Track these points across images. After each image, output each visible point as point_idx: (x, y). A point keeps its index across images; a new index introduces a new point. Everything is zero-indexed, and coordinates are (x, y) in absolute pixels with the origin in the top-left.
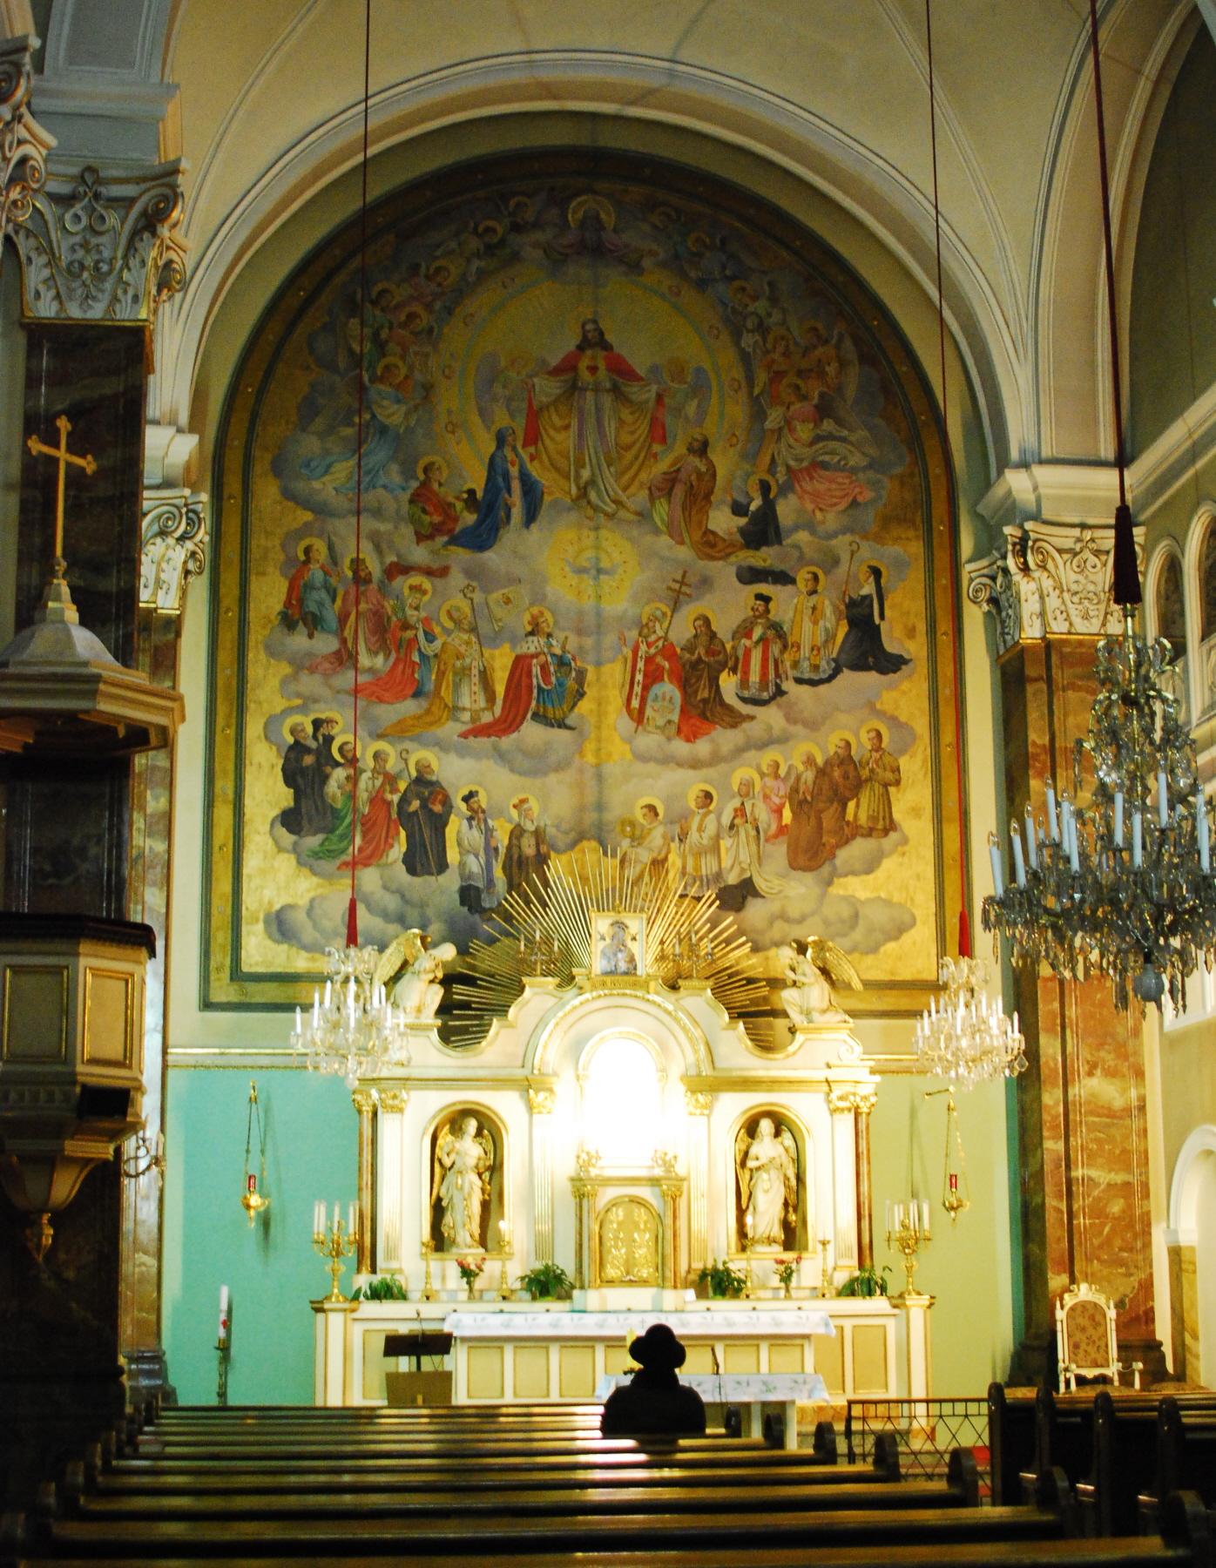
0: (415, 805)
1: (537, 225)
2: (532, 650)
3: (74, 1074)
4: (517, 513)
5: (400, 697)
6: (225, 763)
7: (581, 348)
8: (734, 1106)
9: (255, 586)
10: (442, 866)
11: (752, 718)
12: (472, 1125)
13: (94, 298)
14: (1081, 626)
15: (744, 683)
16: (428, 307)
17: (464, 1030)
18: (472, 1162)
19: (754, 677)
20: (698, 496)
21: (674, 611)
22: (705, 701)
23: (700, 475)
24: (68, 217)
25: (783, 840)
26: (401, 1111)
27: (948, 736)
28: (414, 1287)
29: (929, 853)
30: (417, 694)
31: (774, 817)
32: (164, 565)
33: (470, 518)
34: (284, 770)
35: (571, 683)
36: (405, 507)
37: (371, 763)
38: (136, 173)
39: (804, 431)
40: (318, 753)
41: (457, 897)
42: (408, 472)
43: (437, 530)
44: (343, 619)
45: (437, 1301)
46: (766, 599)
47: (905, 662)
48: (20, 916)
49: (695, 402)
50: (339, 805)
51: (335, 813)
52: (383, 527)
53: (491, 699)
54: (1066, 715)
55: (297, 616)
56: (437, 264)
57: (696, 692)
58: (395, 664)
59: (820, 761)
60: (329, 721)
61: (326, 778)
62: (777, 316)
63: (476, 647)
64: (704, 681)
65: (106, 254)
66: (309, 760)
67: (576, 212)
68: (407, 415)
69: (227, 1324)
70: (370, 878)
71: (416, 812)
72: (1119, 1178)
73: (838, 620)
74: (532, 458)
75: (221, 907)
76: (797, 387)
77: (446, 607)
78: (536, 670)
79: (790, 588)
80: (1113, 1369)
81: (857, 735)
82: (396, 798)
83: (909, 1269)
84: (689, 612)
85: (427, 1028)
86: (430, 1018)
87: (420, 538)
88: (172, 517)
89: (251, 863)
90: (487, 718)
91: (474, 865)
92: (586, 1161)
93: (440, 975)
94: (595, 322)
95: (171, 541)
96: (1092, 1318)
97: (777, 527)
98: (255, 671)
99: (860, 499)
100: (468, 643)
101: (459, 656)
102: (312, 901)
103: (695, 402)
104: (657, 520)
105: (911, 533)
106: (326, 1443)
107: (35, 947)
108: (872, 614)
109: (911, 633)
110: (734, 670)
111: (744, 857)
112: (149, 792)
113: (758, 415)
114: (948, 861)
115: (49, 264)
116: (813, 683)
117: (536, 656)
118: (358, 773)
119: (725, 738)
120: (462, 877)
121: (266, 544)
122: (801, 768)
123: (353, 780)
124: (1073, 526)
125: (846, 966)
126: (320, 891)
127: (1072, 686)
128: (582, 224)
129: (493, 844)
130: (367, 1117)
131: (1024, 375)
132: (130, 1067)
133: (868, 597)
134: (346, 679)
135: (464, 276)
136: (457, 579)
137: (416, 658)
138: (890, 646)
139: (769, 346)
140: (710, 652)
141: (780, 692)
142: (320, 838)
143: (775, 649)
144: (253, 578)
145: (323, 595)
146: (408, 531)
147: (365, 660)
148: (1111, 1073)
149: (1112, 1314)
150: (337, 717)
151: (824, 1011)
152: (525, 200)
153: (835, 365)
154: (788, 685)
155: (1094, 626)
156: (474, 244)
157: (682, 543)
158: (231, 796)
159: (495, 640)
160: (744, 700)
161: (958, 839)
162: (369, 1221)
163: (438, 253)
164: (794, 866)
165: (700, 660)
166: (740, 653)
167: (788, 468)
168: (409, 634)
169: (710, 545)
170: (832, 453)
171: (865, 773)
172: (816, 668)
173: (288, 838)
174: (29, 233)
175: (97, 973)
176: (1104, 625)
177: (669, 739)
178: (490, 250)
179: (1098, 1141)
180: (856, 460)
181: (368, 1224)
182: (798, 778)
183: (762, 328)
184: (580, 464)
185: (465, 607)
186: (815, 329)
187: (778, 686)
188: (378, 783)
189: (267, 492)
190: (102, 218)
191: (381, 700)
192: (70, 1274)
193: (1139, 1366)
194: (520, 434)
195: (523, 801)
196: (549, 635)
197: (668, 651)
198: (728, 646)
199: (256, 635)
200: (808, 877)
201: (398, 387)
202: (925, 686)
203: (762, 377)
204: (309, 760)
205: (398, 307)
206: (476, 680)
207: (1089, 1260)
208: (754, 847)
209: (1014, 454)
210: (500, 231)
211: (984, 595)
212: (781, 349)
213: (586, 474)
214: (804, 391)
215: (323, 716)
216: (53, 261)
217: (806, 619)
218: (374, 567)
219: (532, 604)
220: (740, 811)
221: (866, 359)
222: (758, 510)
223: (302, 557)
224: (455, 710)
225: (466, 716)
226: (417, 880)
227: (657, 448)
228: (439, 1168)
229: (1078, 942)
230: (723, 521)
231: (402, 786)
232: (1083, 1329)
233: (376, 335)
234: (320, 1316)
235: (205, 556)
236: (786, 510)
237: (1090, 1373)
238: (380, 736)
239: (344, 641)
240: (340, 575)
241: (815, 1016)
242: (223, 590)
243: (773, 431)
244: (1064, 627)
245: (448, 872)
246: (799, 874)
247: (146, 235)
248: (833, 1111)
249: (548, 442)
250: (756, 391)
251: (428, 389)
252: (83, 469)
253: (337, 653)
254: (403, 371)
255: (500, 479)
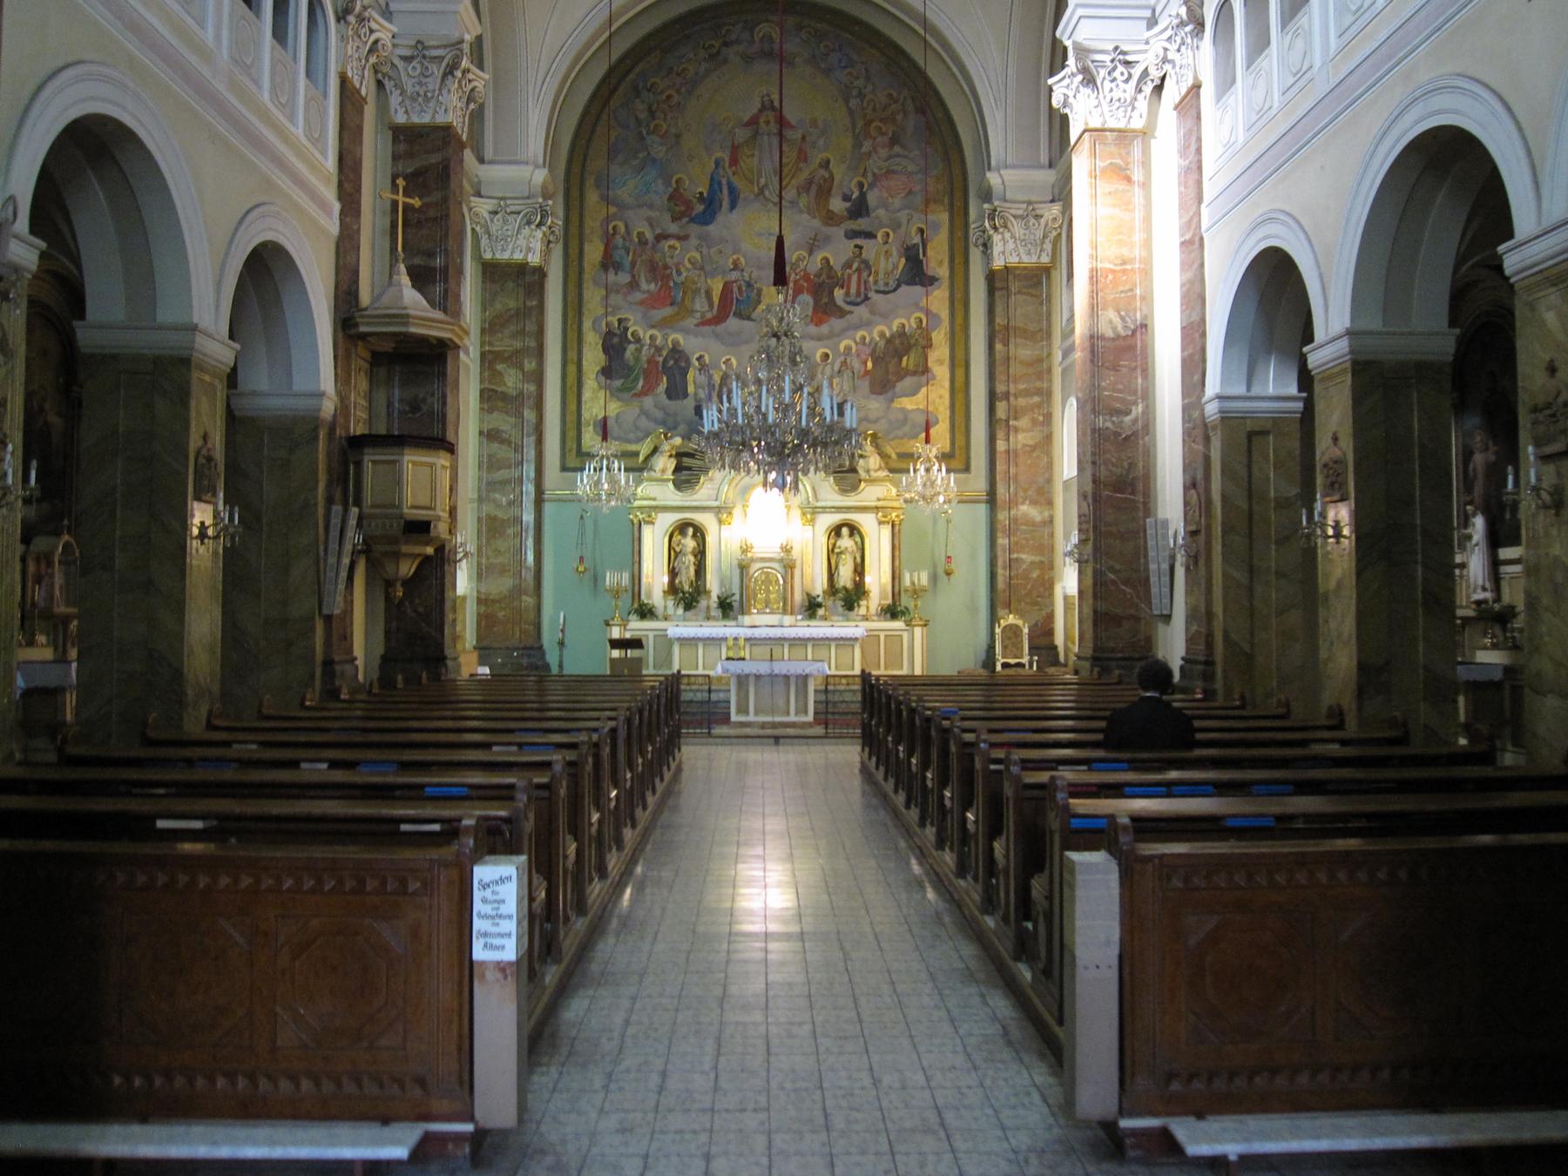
1: (738, 42)
2: (733, 278)
3: (402, 514)
4: (726, 203)
7: (760, 111)
8: (827, 520)
9: (587, 247)
10: (686, 395)
13: (425, 112)
14: (1025, 259)
15: (847, 294)
16: (678, 92)
17: (688, 481)
19: (853, 290)
21: (810, 255)
22: (825, 304)
23: (825, 180)
24: (410, 69)
25: (868, 377)
26: (653, 523)
27: (959, 320)
28: (660, 611)
29: (947, 384)
30: (672, 304)
32: (531, 239)
33: (700, 208)
35: (754, 295)
37: (648, 341)
38: (445, 43)
39: (883, 153)
40: (620, 336)
42: (668, 183)
43: (682, 215)
44: (633, 264)
45: (672, 620)
46: (860, 247)
47: (937, 280)
48: (393, 436)
49: (823, 139)
50: (632, 364)
51: (630, 369)
55: (608, 263)
57: (821, 299)
58: (660, 289)
59: (888, 335)
60: (626, 319)
61: (625, 349)
63: (703, 277)
64: (825, 293)
65: (431, 88)
66: (616, 340)
70: (648, 401)
71: (671, 367)
72: (1037, 559)
73: (900, 257)
74: (734, 174)
75: (571, 418)
76: (880, 128)
78: (735, 289)
79: (873, 241)
80: (1025, 660)
81: (909, 322)
82: (661, 359)
84: (819, 257)
85: (668, 480)
87: (674, 219)
88: (533, 214)
89: (587, 394)
90: (709, 316)
93: (674, 453)
95: (533, 227)
96: (1015, 633)
97: (867, 207)
98: (587, 294)
100: (699, 276)
101: (694, 283)
102: (618, 414)
103: (823, 139)
104: (801, 205)
110: (842, 287)
112: (526, 361)
113: (858, 145)
114: (569, 425)
115: (401, 94)
117: (735, 282)
118: (643, 346)
119: (836, 323)
120: (696, 400)
121: (593, 223)
123: (639, 350)
125: (888, 447)
126: (623, 409)
128: (762, 40)
129: (712, 382)
130: (636, 526)
131: (999, 117)
132: (434, 509)
133: (916, 245)
134: (638, 296)
135: (697, 74)
136: (694, 242)
137: (672, 284)
139: (865, 105)
140: (829, 277)
141: (867, 298)
142: (622, 381)
143: (865, 275)
145: (622, 252)
146: (667, 217)
147: (644, 286)
148: (1034, 503)
149: (1026, 630)
150: (631, 317)
152: (731, 27)
154: (871, 294)
155: (1034, 259)
156: (702, 54)
157: (815, 217)
159: (712, 274)
160: (849, 303)
161: (963, 376)
162: (636, 578)
163: (684, 60)
166: (846, 277)
167: (874, 175)
168: (668, 271)
169: (831, 219)
171: (913, 341)
172: (887, 284)
173: (602, 379)
175: (414, 463)
178: (712, 57)
179: (1027, 540)
180: (911, 168)
181: (637, 582)
182: (876, 344)
183: (861, 95)
184: (760, 176)
185: (698, 256)
186: (891, 95)
187: (866, 295)
189: (592, 197)
191: (654, 308)
192: (421, 610)
193: (1036, 658)
194: (727, 159)
195: (729, 360)
196: (743, 270)
200: (881, 398)
201: (662, 137)
202: (947, 294)
203: (860, 124)
204: (616, 340)
205: (662, 92)
209: (993, 163)
212: (870, 107)
214: (884, 130)
215: (623, 317)
217: (882, 259)
218: (649, 235)
219: (734, 254)
220: (844, 363)
221: (921, 111)
222: (857, 197)
223: (611, 232)
224: (692, 312)
225: (699, 315)
226: (671, 402)
227: (801, 165)
228: (674, 553)
229: (819, 449)
230: (837, 205)
231: (665, 353)
233: (650, 108)
235: (559, 230)
236: (872, 198)
237: (1013, 661)
238: (653, 327)
239: (633, 276)
240: (631, 240)
242: (571, 251)
243: (865, 154)
244: (1017, 260)
246: (874, 396)
247: (450, 77)
249: (742, 164)
250: (857, 131)
252: (413, 205)
253: (630, 283)
254: (665, 127)
255: (716, 186)
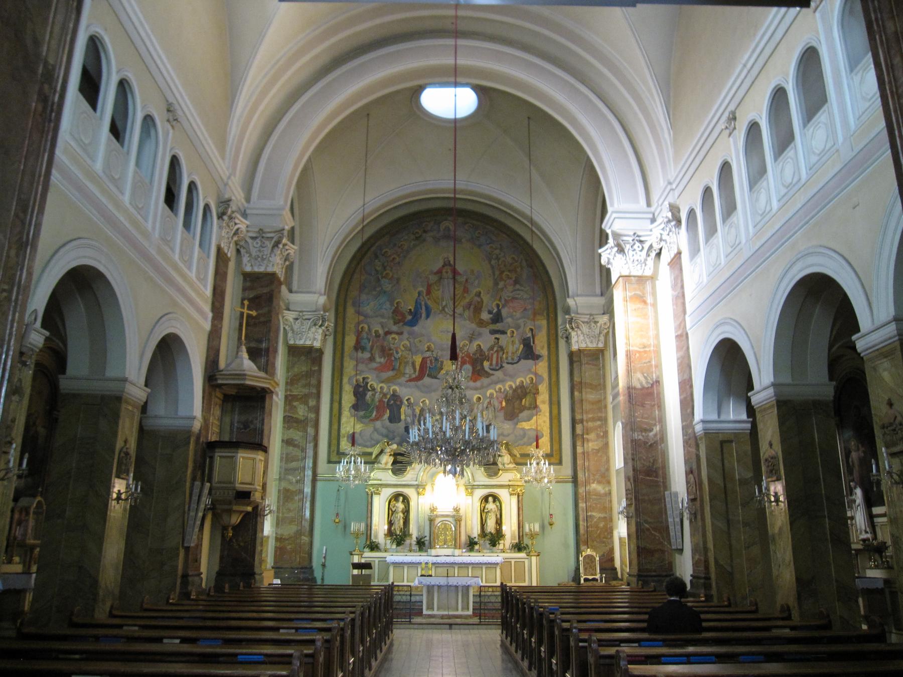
0: (392, 402)
2: (427, 356)
4: (424, 315)
5: (389, 370)
6: (337, 390)
8: (480, 493)
10: (400, 420)
11: (493, 375)
12: (401, 499)
13: (261, 265)
15: (491, 364)
17: (400, 470)
18: (400, 510)
19: (494, 362)
20: (478, 309)
21: (470, 343)
22: (479, 370)
23: (478, 302)
24: (255, 243)
25: (503, 411)
26: (379, 494)
27: (554, 379)
29: (548, 414)
30: (393, 369)
31: (500, 404)
33: (409, 317)
34: (354, 392)
36: (391, 315)
37: (379, 390)
39: (510, 288)
41: (404, 430)
43: (399, 321)
45: (388, 552)
51: (368, 406)
52: (384, 320)
53: (415, 371)
54: (585, 373)
55: (358, 347)
56: (402, 243)
57: (476, 367)
59: (514, 387)
60: (368, 378)
61: (366, 395)
62: (502, 254)
65: (265, 253)
66: (361, 389)
67: (442, 227)
68: (392, 287)
69: (325, 557)
70: (378, 424)
72: (602, 515)
75: (335, 433)
77: (402, 343)
78: (428, 362)
81: (526, 380)
82: (386, 400)
83: (532, 544)
85: (389, 469)
86: (389, 466)
87: (395, 323)
90: (414, 376)
91: (409, 420)
92: (433, 510)
93: (392, 453)
94: (448, 258)
95: (317, 327)
96: (591, 560)
98: (346, 364)
99: (527, 308)
100: (409, 354)
101: (406, 358)
102: (361, 431)
105: (543, 318)
106: (543, 599)
107: (226, 450)
108: (530, 343)
109: (543, 348)
111: (490, 416)
116: (512, 364)
117: (429, 357)
119: (485, 381)
121: (350, 326)
122: (508, 389)
123: (374, 395)
124: (587, 315)
127: (587, 363)
133: (529, 337)
134: (374, 365)
136: (406, 335)
137: (393, 359)
138: (537, 353)
141: (502, 367)
143: (501, 353)
144: (346, 336)
146: (392, 322)
147: (378, 360)
148: (599, 482)
149: (598, 559)
151: (508, 464)
153: (520, 268)
156: (413, 237)
158: (338, 400)
159: (416, 353)
160: (491, 369)
163: (402, 240)
164: (506, 419)
165: (478, 358)
167: (505, 300)
168: (391, 352)
169: (481, 323)
170: (519, 294)
171: (528, 391)
172: (513, 359)
174: (244, 248)
175: (243, 458)
176: (597, 344)
177: (468, 381)
178: (417, 238)
183: (498, 259)
184: (443, 300)
188: (381, 396)
189: (350, 311)
190: (264, 243)
191: (382, 371)
193: (604, 575)
196: (433, 351)
197: (468, 355)
198: (486, 354)
199: (346, 354)
200: (510, 422)
203: (497, 273)
204: (361, 389)
205: (390, 256)
206: (411, 365)
207: (593, 541)
208: (493, 414)
210: (420, 232)
211: (564, 336)
213: (444, 303)
215: (365, 376)
216: (250, 255)
218: (381, 332)
220: (490, 403)
223: (360, 330)
226: (392, 424)
227: (465, 295)
228: (391, 512)
230: (485, 316)
231: (388, 396)
232: (588, 563)
233: (383, 265)
234: (352, 556)
236: (504, 312)
237: (590, 577)
238: (382, 382)
239: (372, 354)
241: (506, 466)
245: (401, 423)
248: (511, 494)
250: (496, 277)
251: (398, 280)
253: (370, 357)
254: (391, 274)
